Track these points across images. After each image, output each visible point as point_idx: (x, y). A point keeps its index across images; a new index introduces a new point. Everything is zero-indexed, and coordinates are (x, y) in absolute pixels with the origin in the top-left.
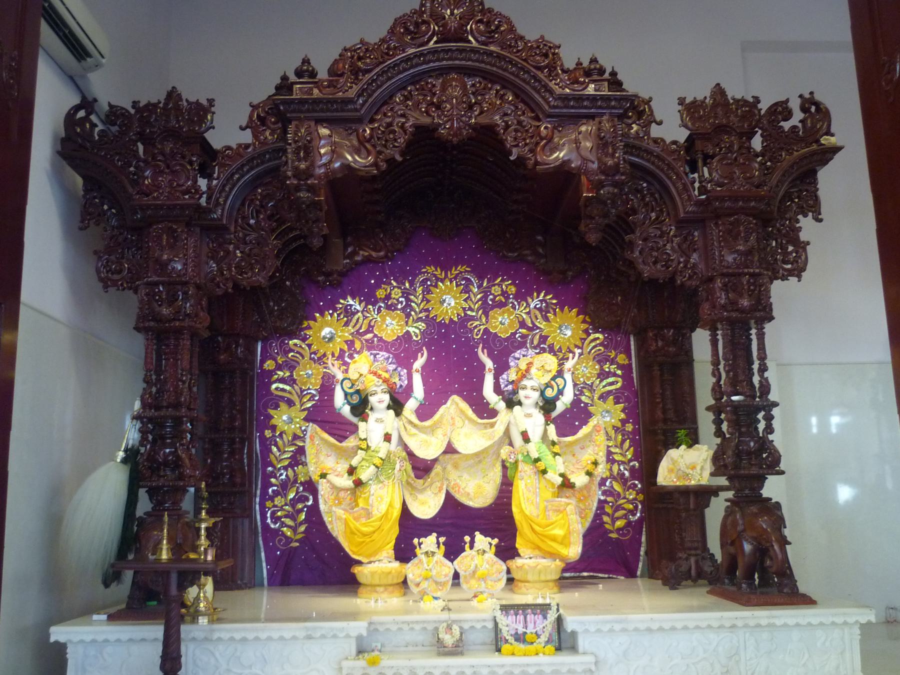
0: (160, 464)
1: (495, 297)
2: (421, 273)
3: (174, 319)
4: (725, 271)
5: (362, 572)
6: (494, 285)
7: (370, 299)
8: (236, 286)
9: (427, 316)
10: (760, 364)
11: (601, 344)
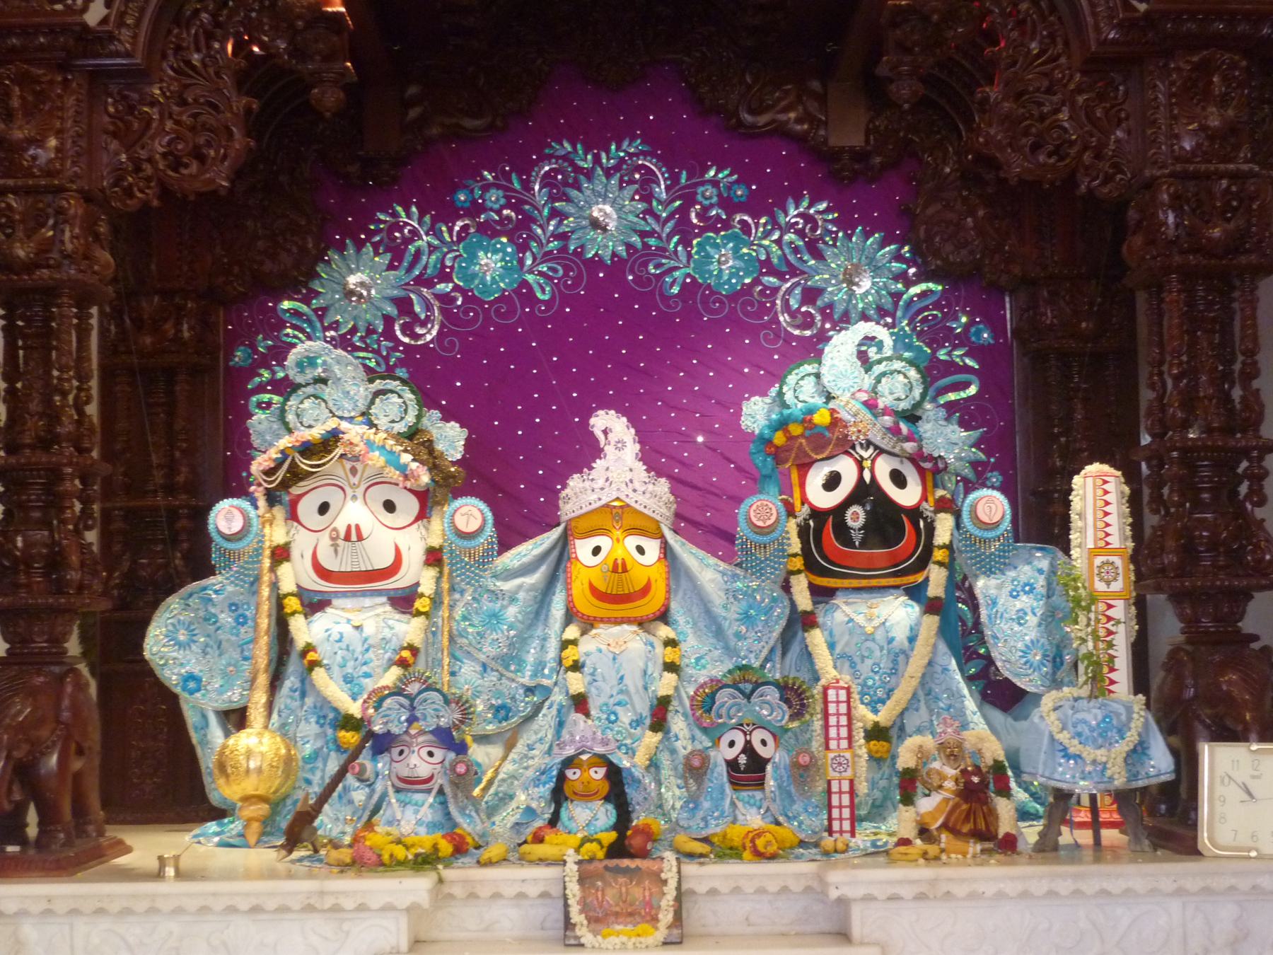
0: (16, 561)
1: (706, 209)
2: (545, 158)
3: (39, 266)
4: (1178, 167)
5: (376, 828)
6: (703, 183)
7: (441, 210)
8: (165, 192)
9: (564, 249)
10: (1244, 363)
11: (937, 305)
